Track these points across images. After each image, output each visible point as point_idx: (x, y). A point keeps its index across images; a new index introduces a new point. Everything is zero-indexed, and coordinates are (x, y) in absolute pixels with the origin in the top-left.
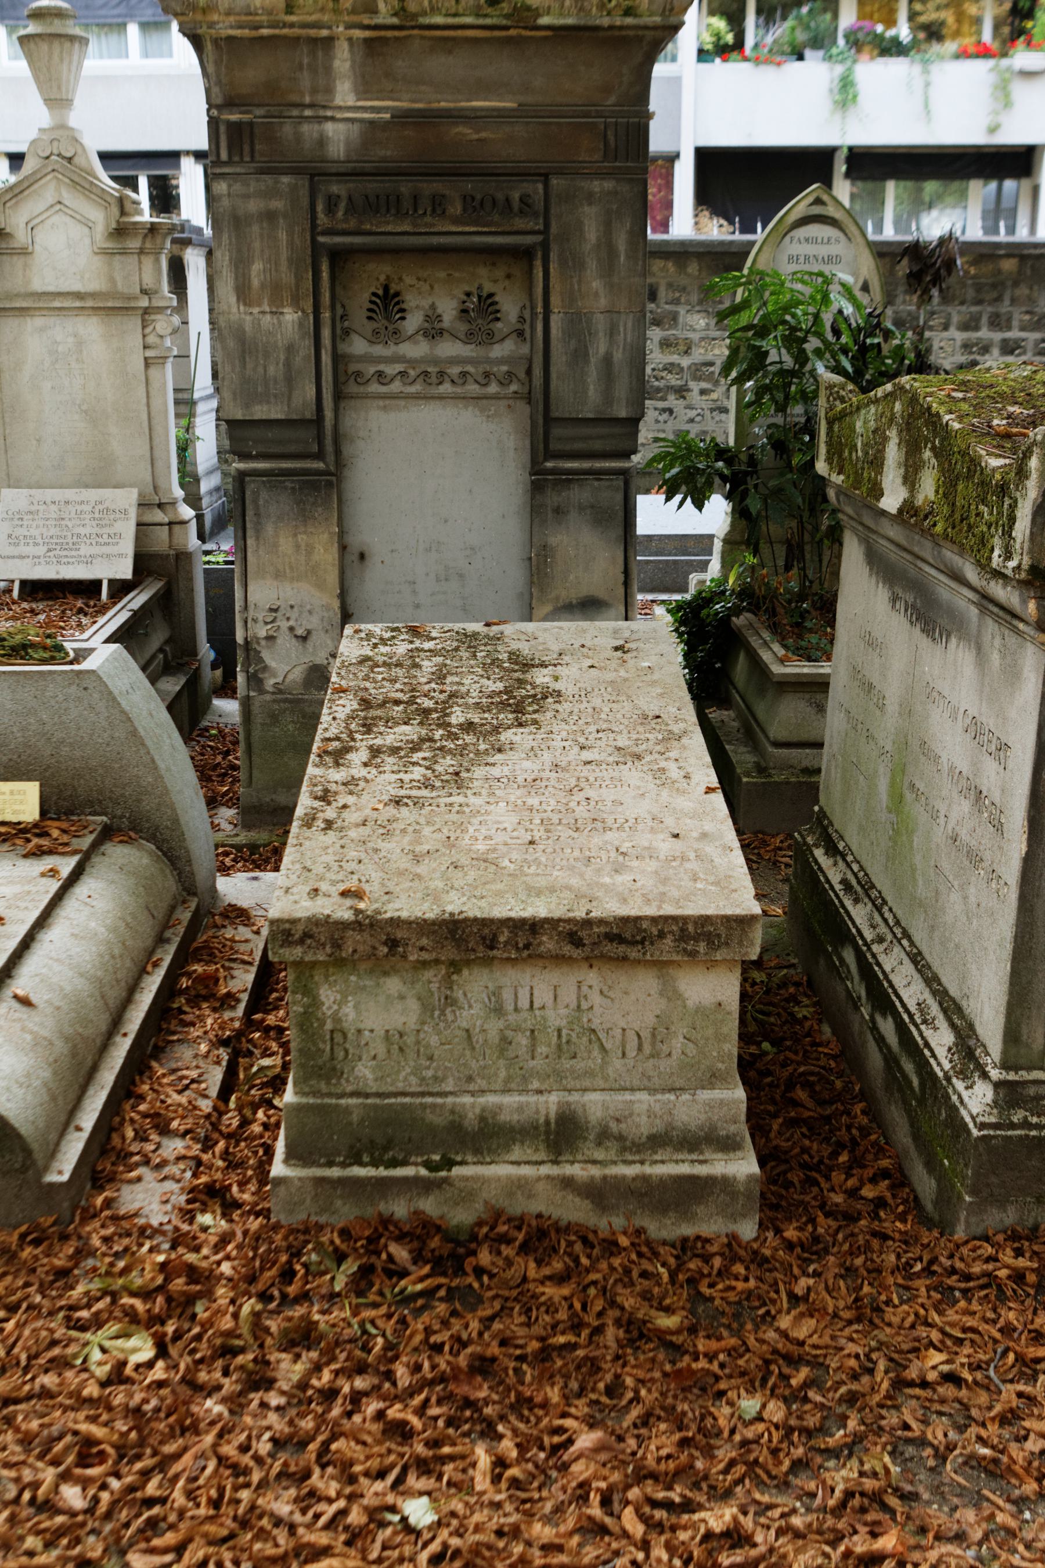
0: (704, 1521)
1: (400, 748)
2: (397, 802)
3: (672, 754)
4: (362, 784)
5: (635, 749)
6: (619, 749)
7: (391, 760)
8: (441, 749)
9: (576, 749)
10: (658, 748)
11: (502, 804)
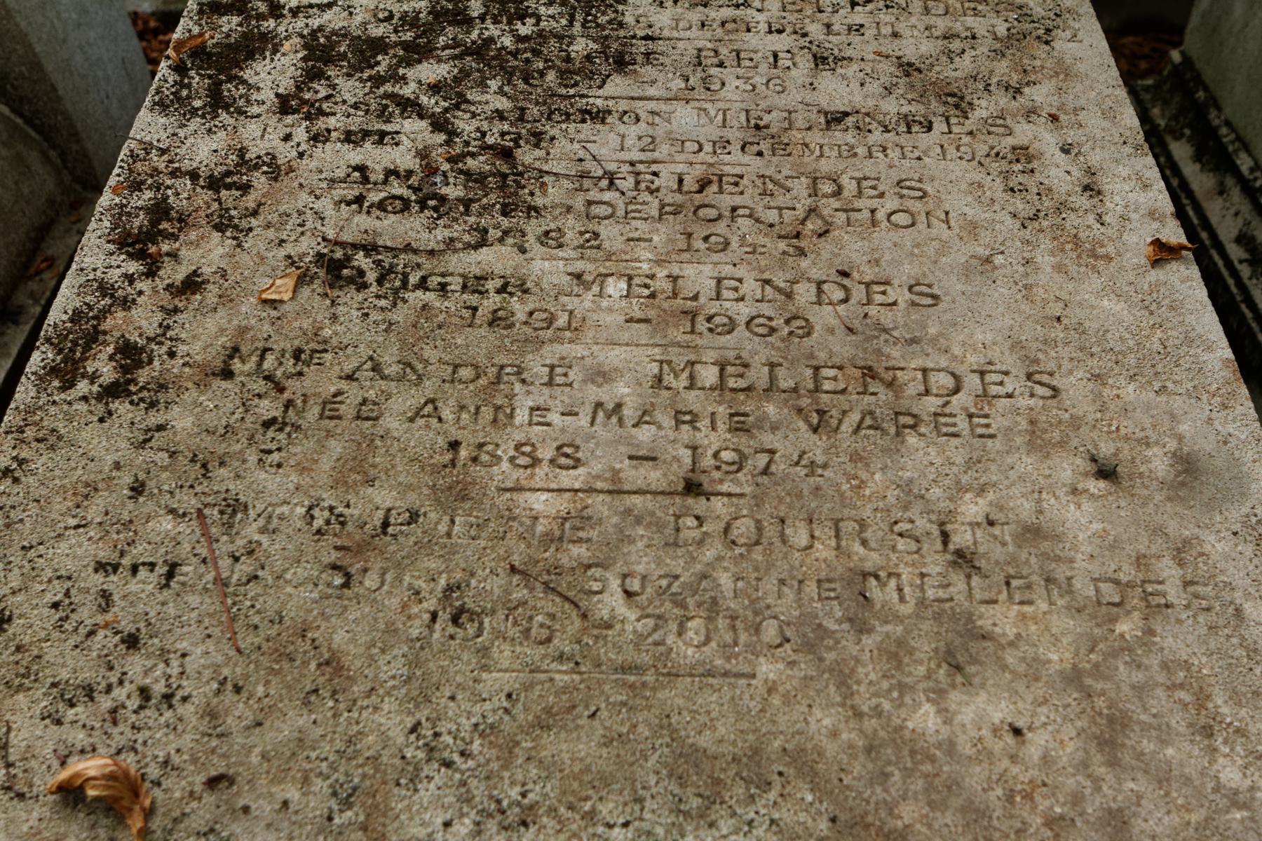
0: (572, 623)
1: (379, 45)
2: (335, 269)
3: (1040, 94)
4: (259, 180)
5: (946, 71)
6: (907, 68)
7: (350, 89)
8: (480, 50)
9: (805, 62)
10: (1002, 68)
11: (616, 287)
